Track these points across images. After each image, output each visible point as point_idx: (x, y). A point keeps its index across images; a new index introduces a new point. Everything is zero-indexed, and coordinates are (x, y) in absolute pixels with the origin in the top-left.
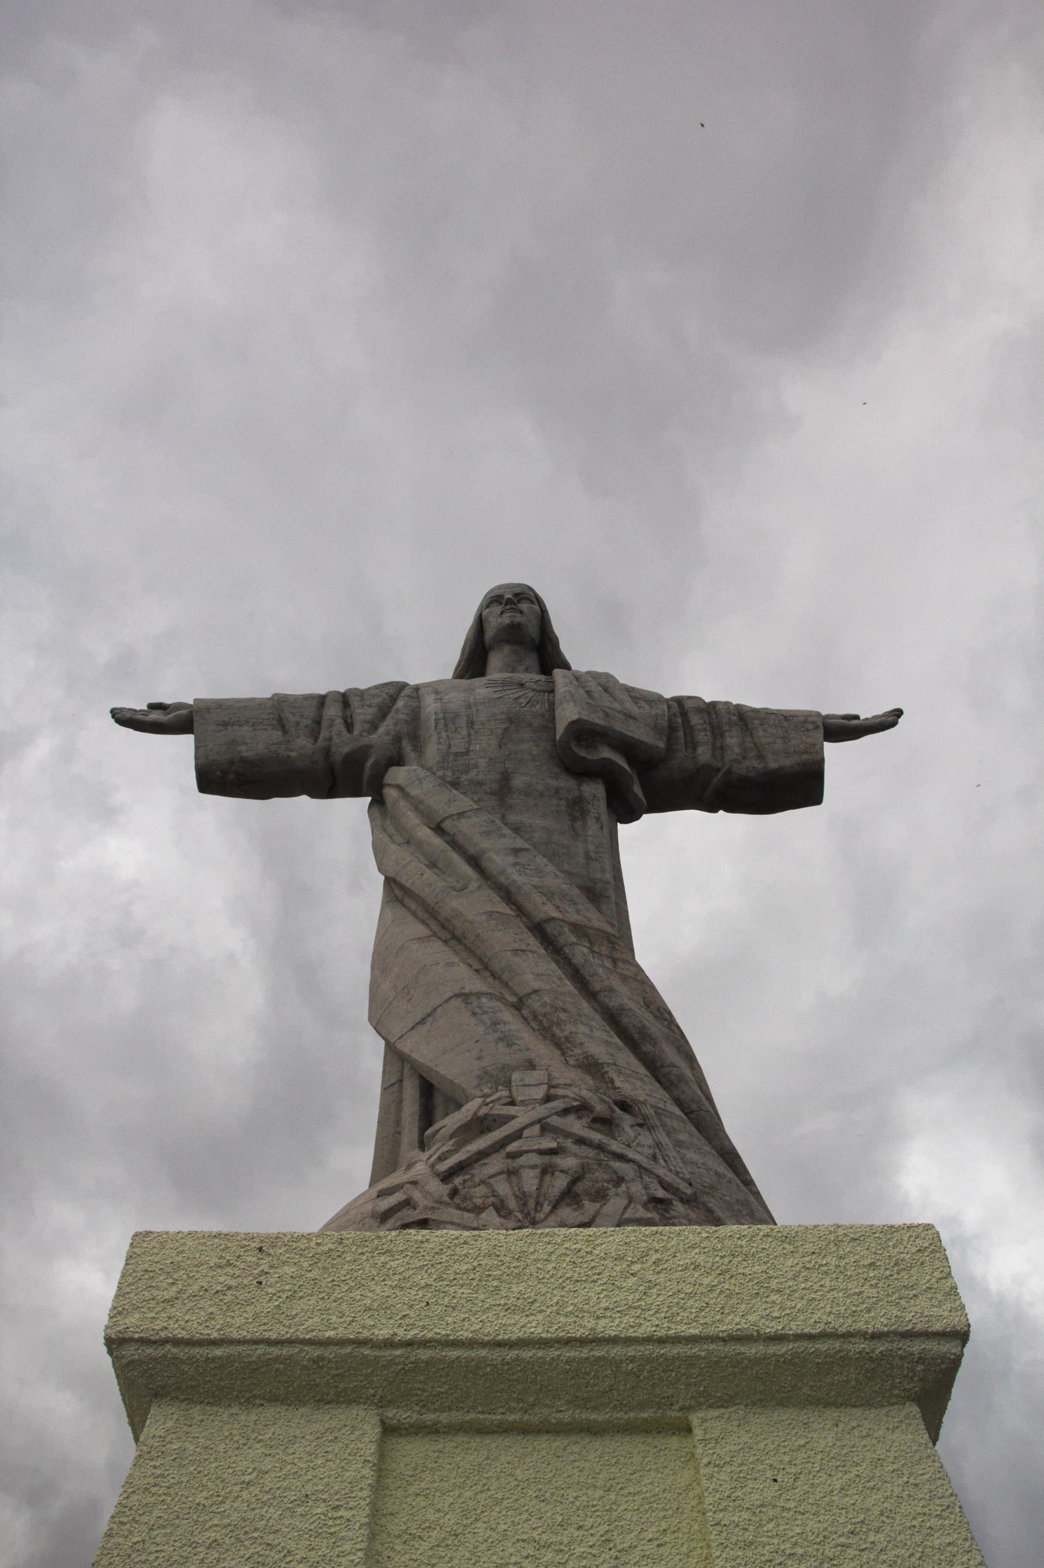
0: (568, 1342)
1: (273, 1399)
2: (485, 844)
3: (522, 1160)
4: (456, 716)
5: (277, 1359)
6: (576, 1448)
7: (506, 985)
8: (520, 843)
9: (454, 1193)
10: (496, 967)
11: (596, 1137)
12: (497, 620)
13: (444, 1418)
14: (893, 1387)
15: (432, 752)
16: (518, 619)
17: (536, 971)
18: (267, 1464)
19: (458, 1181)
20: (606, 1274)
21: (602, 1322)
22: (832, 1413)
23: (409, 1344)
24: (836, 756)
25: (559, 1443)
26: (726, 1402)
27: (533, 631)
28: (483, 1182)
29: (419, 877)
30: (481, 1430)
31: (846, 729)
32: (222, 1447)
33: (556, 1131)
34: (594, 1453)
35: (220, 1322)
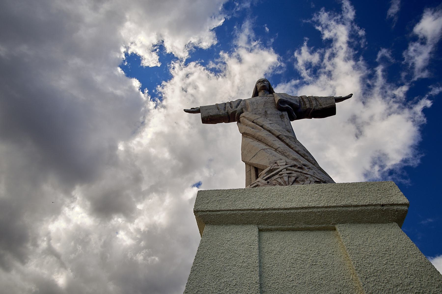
0: (303, 208)
1: (232, 224)
2: (264, 123)
3: (283, 175)
4: (254, 102)
5: (233, 214)
6: (307, 234)
7: (272, 147)
8: (271, 122)
9: (268, 182)
10: (269, 144)
11: (299, 170)
12: (260, 85)
13: (273, 227)
14: (389, 218)
15: (250, 109)
16: (264, 84)
17: (278, 144)
18: (233, 237)
19: (269, 180)
20: (309, 194)
21: (310, 204)
22: (373, 225)
23: (263, 210)
24: (338, 105)
25: (302, 233)
26: (343, 223)
27: (268, 87)
28: (275, 180)
29: (249, 130)
30: (283, 230)
31: (340, 99)
32: (222, 234)
33: (289, 170)
34: (312, 234)
35: (219, 207)
